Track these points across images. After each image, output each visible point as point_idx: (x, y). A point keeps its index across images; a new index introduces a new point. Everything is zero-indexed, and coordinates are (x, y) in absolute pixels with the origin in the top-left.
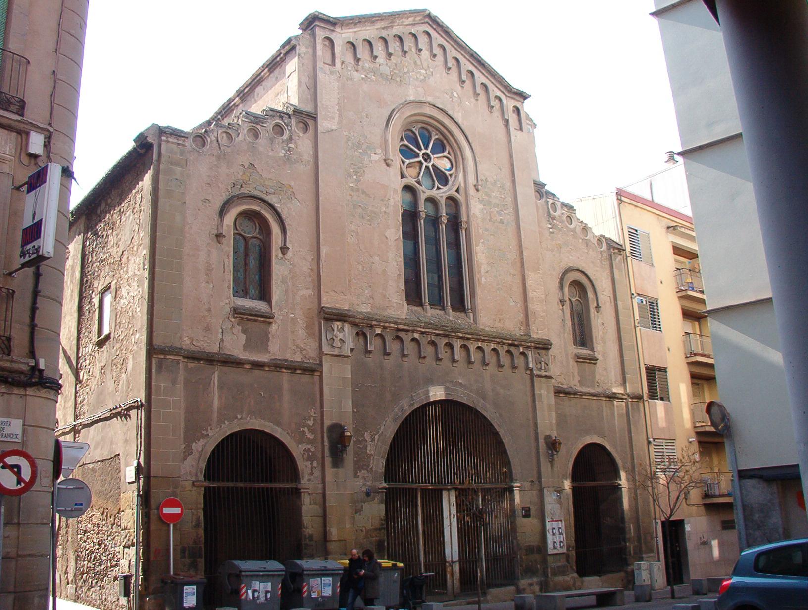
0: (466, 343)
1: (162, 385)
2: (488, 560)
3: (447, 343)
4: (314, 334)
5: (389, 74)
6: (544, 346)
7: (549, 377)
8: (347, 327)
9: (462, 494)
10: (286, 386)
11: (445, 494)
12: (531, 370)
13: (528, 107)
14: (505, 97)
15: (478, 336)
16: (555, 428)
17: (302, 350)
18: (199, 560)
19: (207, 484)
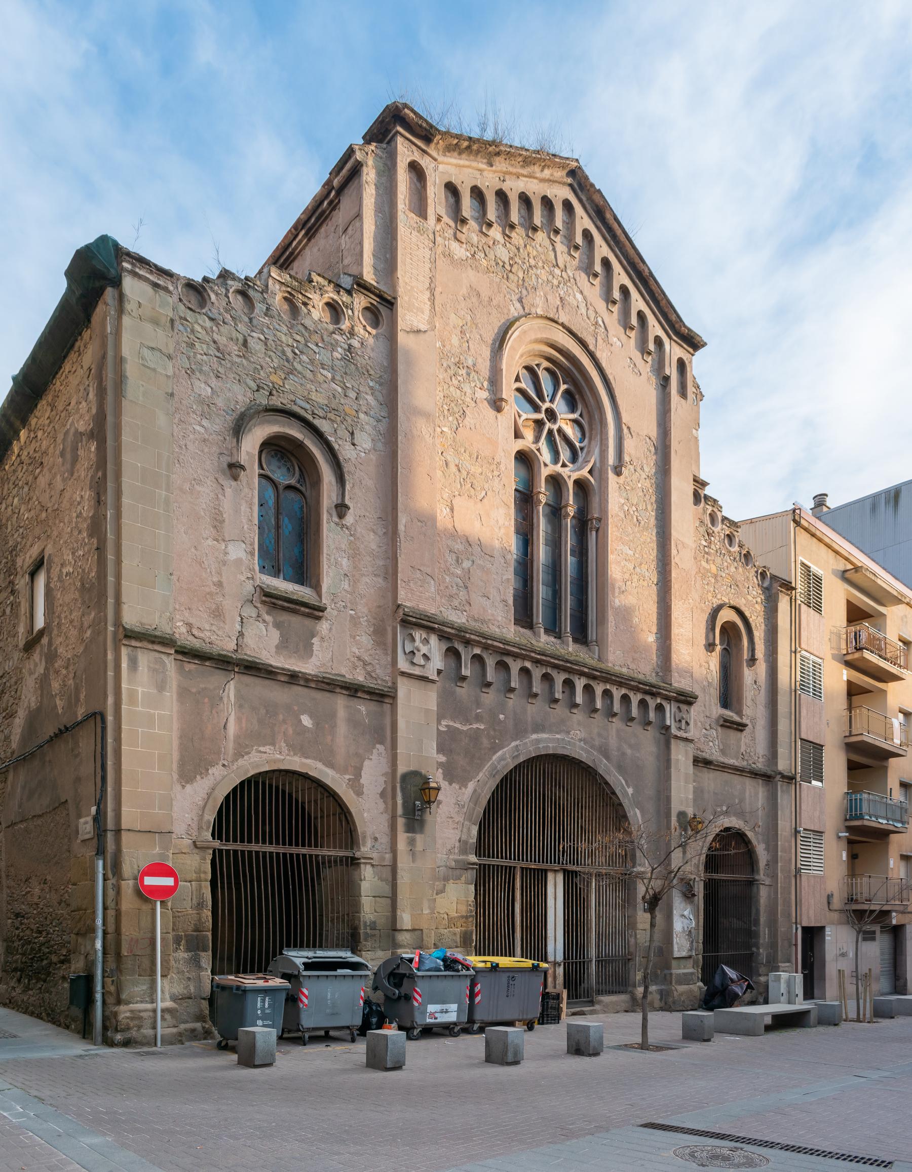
0: (592, 683)
1: (140, 689)
2: (599, 961)
3: (566, 679)
4: (385, 644)
5: (507, 261)
6: (686, 699)
7: (691, 741)
8: (434, 639)
9: (570, 877)
10: (341, 713)
11: (550, 876)
12: (669, 728)
13: (699, 363)
14: (669, 340)
15: (608, 677)
16: (691, 804)
17: (365, 664)
18: (203, 954)
19: (217, 844)
